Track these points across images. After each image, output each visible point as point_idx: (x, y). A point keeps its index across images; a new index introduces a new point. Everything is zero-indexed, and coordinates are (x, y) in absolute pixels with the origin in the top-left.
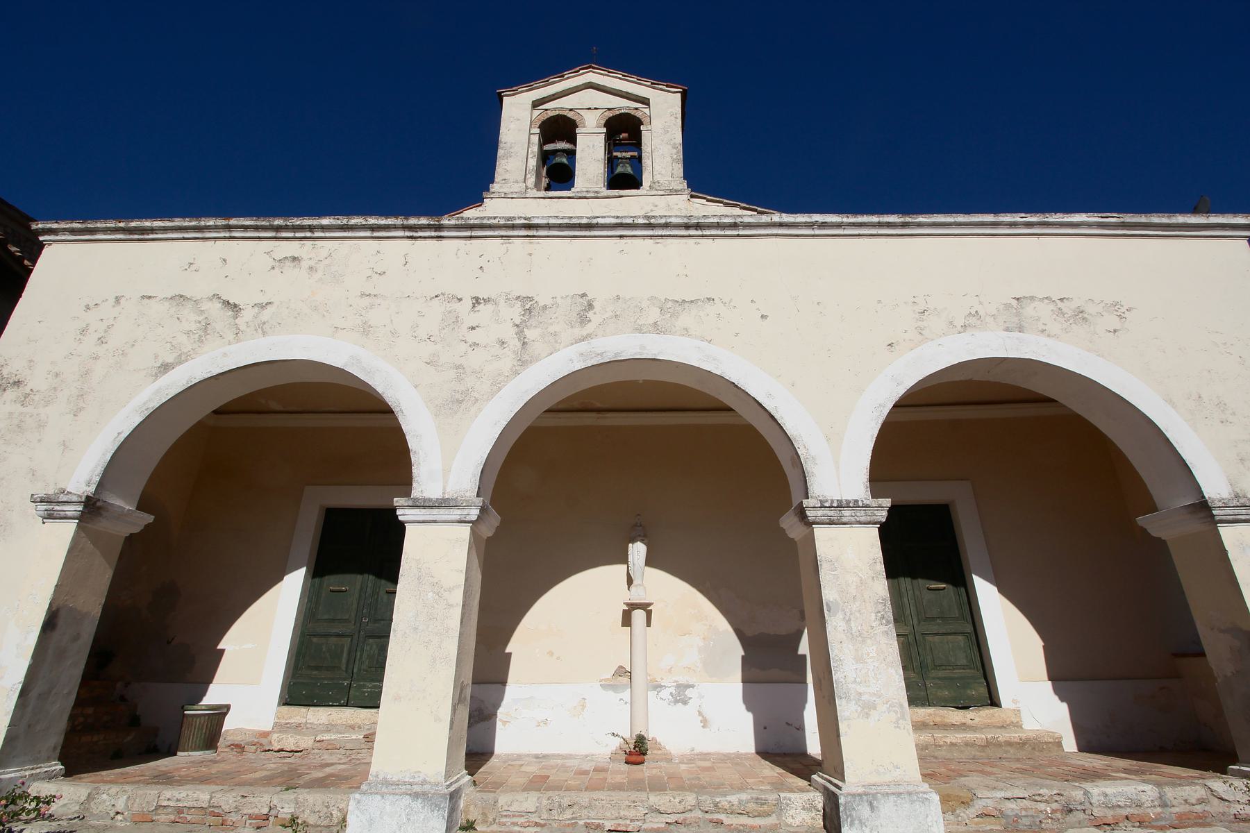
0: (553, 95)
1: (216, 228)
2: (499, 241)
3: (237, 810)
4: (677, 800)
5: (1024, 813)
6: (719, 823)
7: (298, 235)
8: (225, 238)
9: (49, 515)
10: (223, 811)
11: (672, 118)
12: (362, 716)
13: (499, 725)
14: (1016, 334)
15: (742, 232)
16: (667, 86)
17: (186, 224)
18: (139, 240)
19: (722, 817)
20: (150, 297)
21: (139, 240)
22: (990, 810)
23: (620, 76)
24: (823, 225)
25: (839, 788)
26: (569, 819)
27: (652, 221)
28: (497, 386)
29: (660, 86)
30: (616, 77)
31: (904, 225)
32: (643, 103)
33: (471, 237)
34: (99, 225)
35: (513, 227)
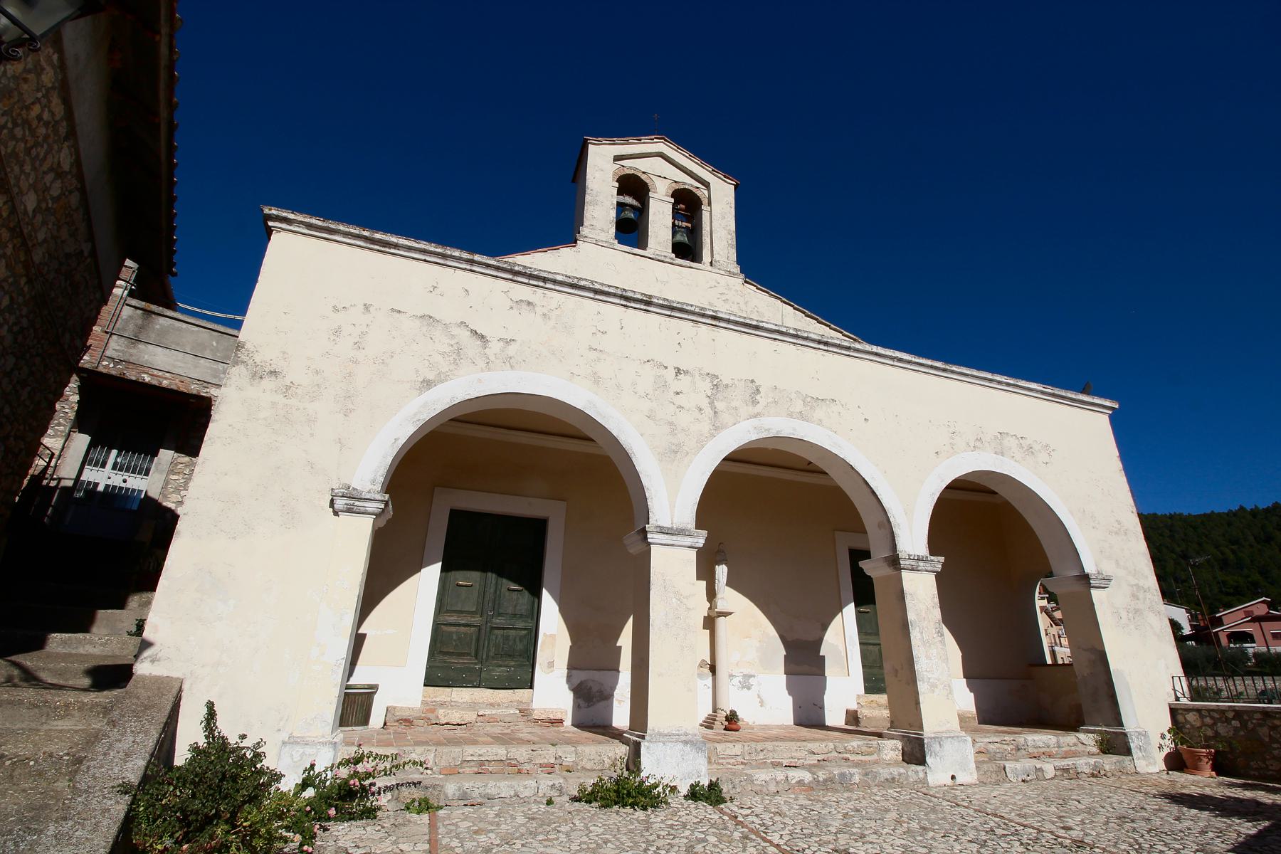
0: (631, 155)
1: (460, 259)
2: (691, 324)
3: (530, 761)
4: (823, 746)
5: (998, 751)
6: (846, 759)
7: (531, 282)
8: (465, 269)
9: (349, 509)
10: (518, 762)
11: (728, 206)
12: (500, 695)
13: (615, 703)
14: (1000, 457)
15: (851, 354)
16: (725, 176)
17: (432, 249)
18: (378, 251)
19: (848, 756)
20: (400, 311)
21: (378, 251)
22: (981, 750)
23: (687, 155)
24: (900, 360)
25: (922, 735)
26: (762, 759)
27: (799, 333)
28: (701, 444)
29: (719, 175)
30: (684, 155)
31: (944, 370)
32: (705, 186)
33: (670, 316)
34: (341, 228)
35: (703, 316)
